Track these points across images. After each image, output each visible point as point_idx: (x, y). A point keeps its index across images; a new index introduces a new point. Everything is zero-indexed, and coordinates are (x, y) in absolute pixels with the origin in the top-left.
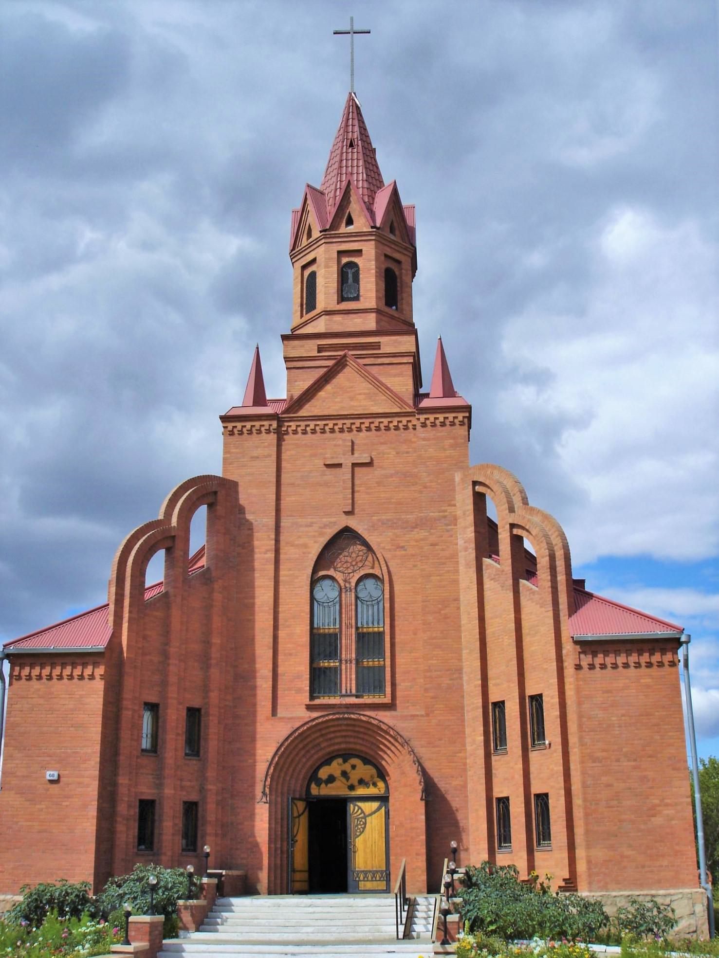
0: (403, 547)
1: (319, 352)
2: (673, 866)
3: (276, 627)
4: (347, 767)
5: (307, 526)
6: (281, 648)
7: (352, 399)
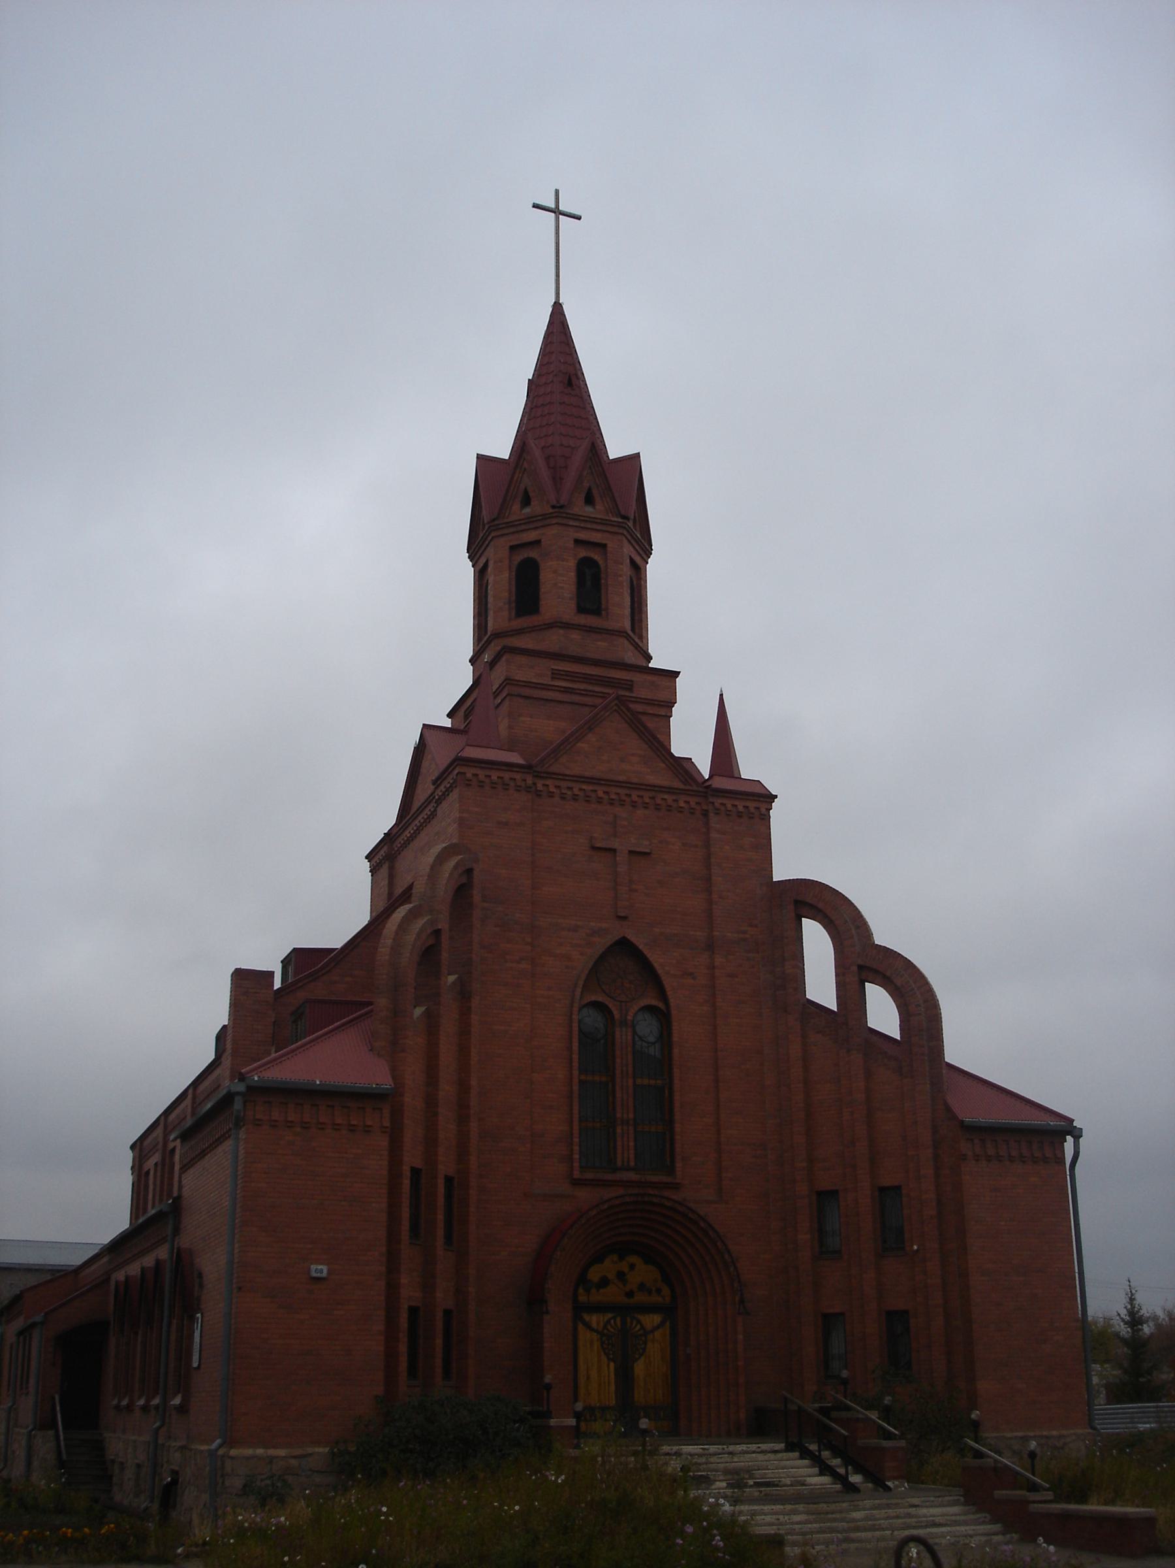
0: (691, 974)
1: (553, 678)
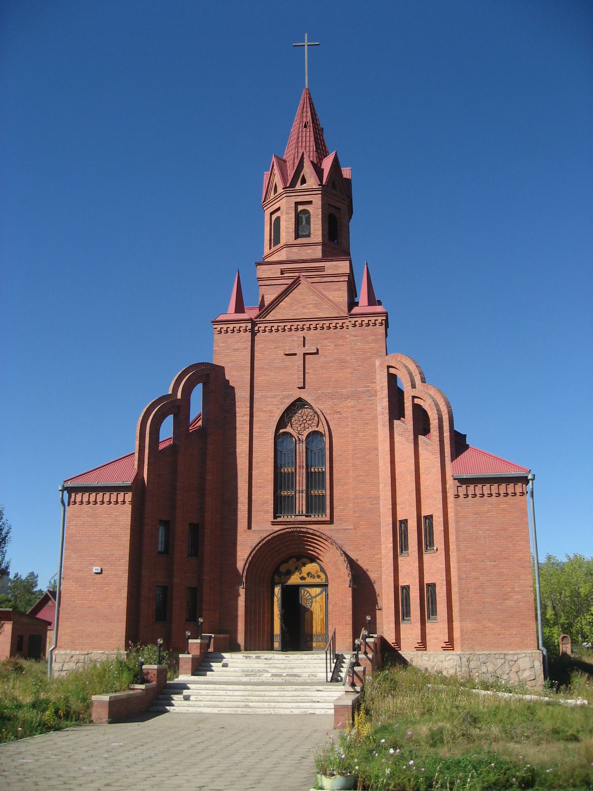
7: (304, 307)
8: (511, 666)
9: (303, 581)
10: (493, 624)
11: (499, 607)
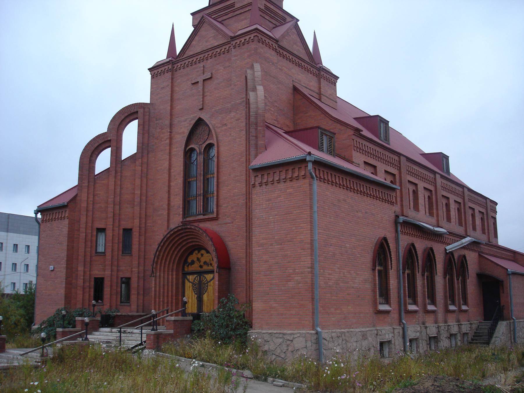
2: (298, 315)
3: (169, 181)
4: (199, 256)
5: (184, 121)
6: (172, 191)
7: (206, 42)
8: (288, 346)
9: (202, 269)
10: (277, 305)
11: (283, 288)
